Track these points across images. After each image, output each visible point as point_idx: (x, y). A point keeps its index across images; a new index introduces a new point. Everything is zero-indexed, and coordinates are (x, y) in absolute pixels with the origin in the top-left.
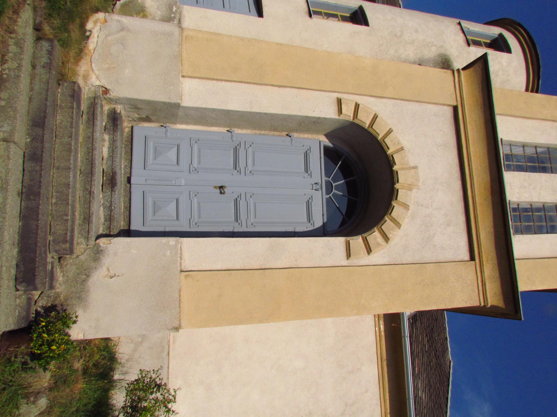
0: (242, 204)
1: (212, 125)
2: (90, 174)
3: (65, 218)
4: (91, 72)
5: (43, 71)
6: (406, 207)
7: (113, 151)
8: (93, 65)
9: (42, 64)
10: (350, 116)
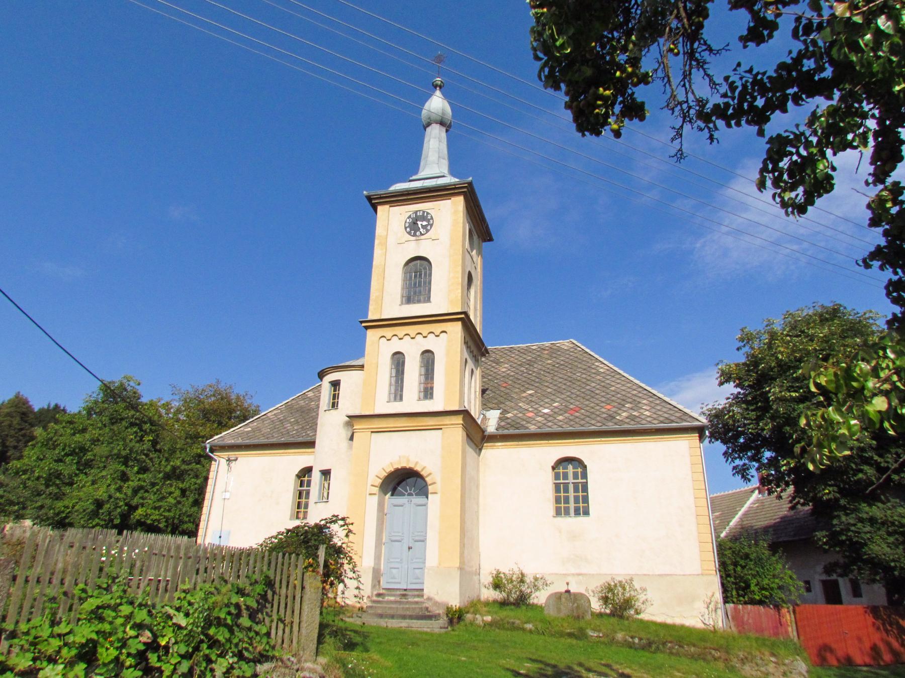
0: (417, 538)
1: (381, 552)
2: (400, 603)
6: (417, 463)
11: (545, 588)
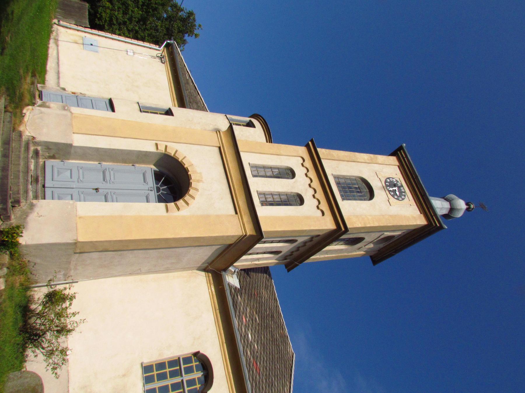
1: (90, 160)
3: (18, 184)
4: (26, 130)
5: (8, 124)
7: (37, 167)
8: (27, 127)
9: (8, 121)
10: (163, 151)
11: (50, 368)
